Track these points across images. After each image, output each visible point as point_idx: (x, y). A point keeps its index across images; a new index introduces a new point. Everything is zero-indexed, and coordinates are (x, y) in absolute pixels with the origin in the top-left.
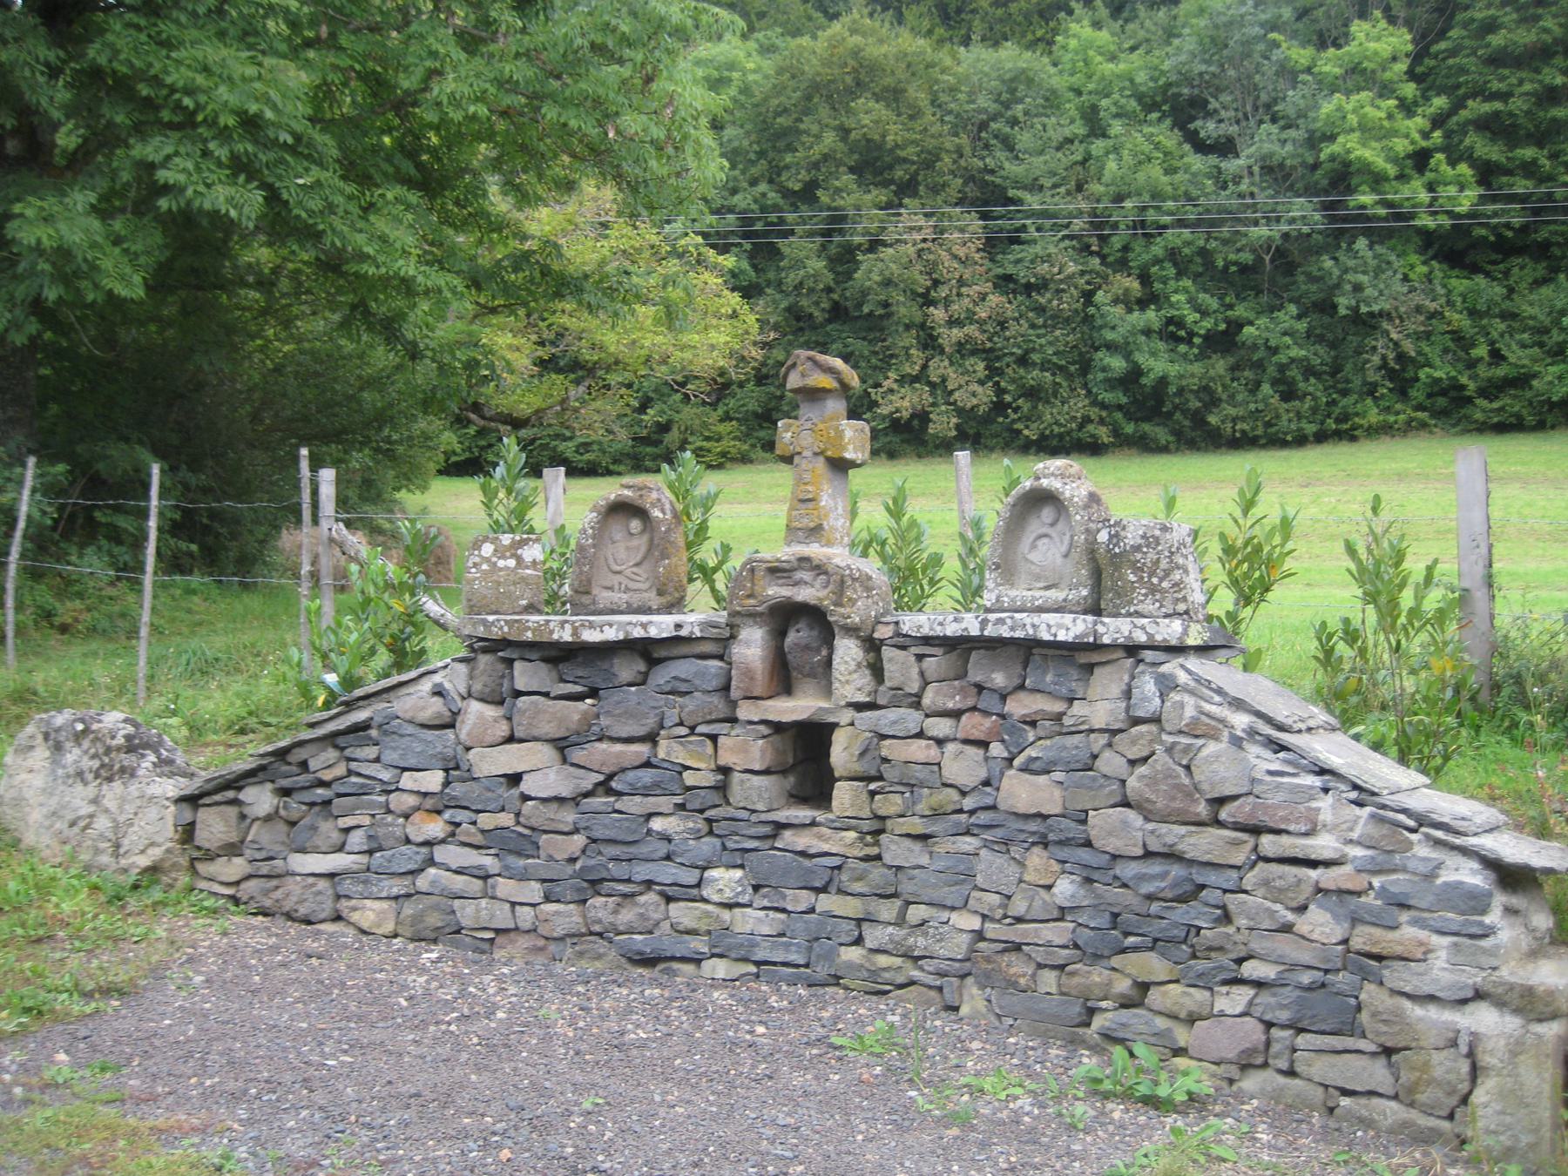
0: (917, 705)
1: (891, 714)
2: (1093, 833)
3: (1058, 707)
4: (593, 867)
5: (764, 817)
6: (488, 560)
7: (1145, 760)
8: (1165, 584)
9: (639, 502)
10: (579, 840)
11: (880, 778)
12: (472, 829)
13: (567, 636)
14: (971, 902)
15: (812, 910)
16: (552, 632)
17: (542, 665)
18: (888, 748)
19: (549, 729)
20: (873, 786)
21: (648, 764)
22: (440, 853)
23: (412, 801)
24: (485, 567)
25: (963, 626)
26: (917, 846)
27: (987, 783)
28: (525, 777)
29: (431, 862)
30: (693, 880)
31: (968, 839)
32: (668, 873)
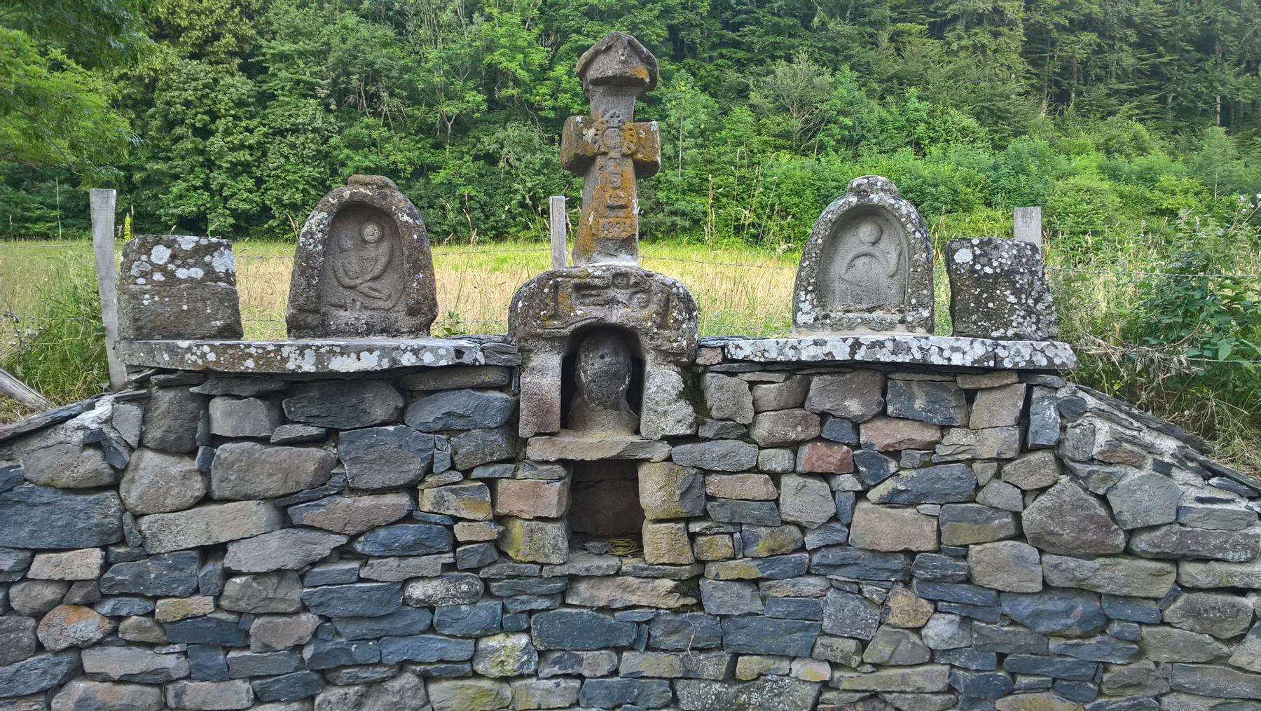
0: (746, 437)
1: (719, 448)
2: (977, 569)
3: (930, 435)
4: (329, 653)
5: (558, 571)
6: (162, 269)
7: (1043, 490)
8: (1040, 306)
9: (378, 203)
10: (309, 621)
11: (705, 516)
12: (148, 622)
13: (308, 366)
14: (817, 651)
15: (615, 673)
16: (287, 360)
17: (259, 402)
18: (715, 485)
19: (273, 485)
20: (695, 527)
21: (409, 518)
22: (91, 661)
23: (49, 593)
24: (158, 277)
25: (826, 349)
26: (747, 592)
27: (835, 518)
28: (231, 548)
29: (78, 672)
30: (465, 655)
31: (812, 580)
32: (434, 648)
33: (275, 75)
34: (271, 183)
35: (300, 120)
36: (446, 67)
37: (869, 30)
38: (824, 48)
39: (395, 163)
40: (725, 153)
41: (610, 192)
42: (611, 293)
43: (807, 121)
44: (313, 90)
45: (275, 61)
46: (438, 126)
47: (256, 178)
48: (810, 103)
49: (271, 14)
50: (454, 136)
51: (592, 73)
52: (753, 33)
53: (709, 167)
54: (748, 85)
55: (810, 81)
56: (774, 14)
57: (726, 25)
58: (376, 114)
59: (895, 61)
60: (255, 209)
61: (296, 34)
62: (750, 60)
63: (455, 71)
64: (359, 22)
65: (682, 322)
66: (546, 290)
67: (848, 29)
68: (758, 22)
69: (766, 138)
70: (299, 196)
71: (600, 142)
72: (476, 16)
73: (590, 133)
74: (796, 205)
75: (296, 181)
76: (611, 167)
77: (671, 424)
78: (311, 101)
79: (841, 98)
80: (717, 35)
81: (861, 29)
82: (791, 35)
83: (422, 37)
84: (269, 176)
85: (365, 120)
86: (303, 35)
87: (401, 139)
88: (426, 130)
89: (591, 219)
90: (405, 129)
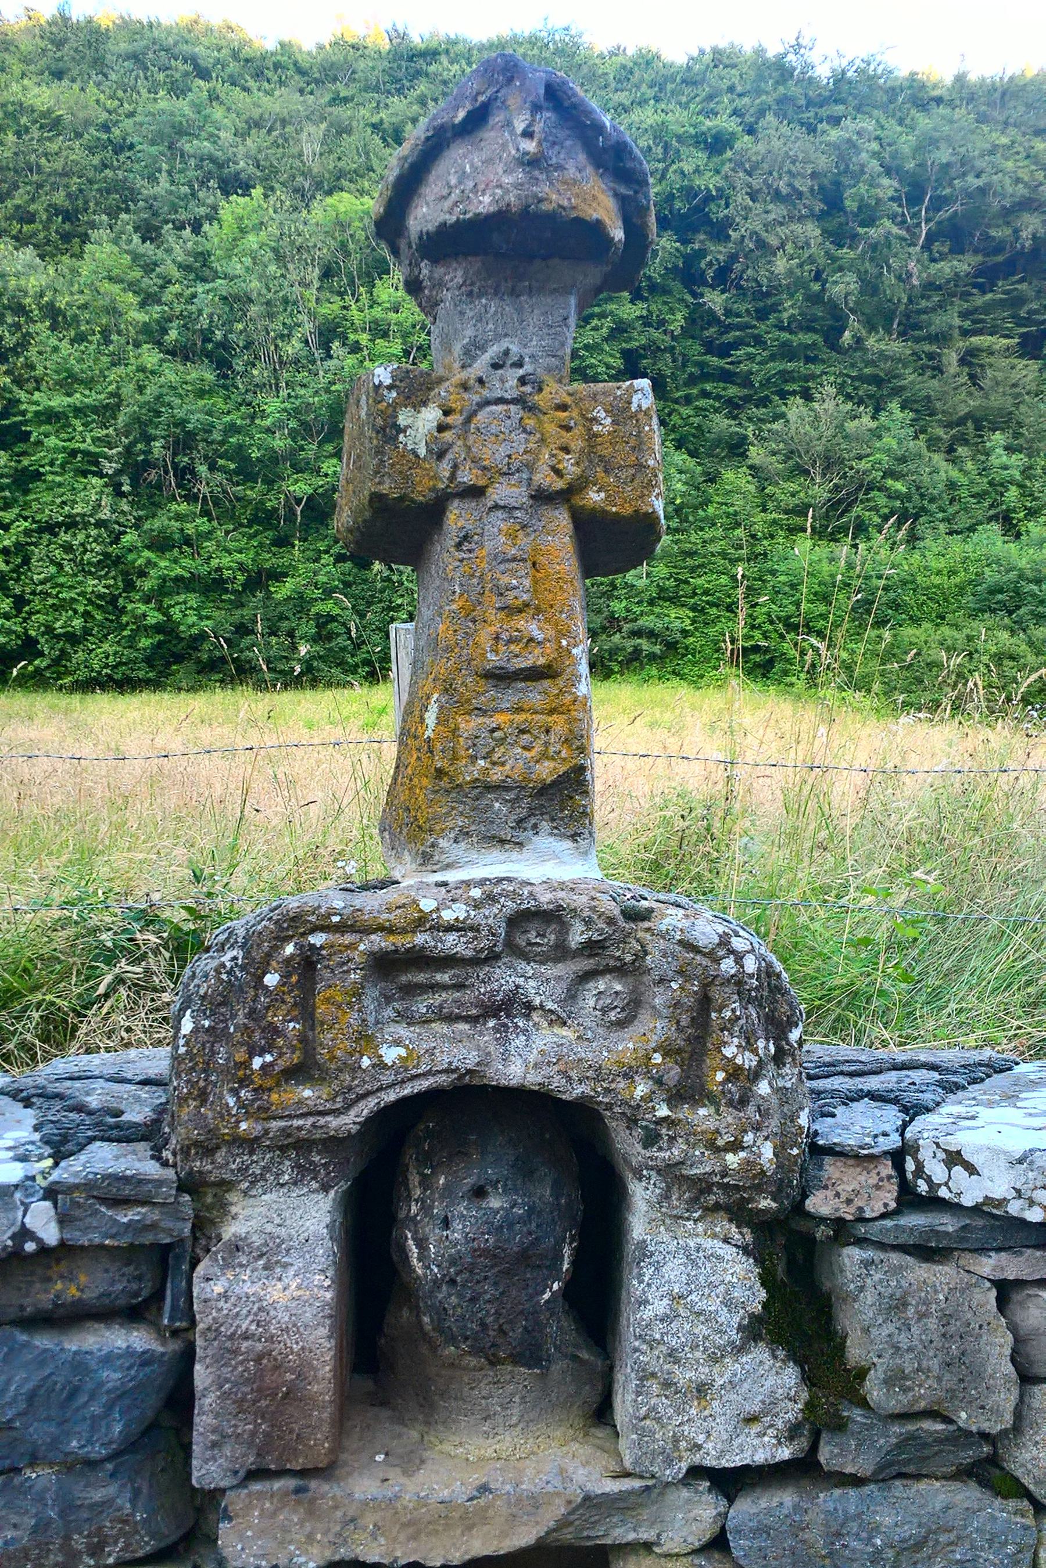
33: (39, 443)
34: (37, 604)
35: (78, 509)
36: (293, 424)
37: (927, 348)
38: (861, 378)
39: (219, 569)
40: (712, 540)
41: (495, 621)
42: (505, 977)
43: (837, 488)
44: (97, 463)
45: (41, 423)
46: (282, 512)
47: (15, 596)
48: (841, 461)
49: (32, 352)
50: (306, 528)
51: (426, 215)
52: (751, 357)
53: (690, 562)
54: (746, 437)
55: (841, 427)
56: (782, 329)
57: (710, 348)
58: (191, 498)
59: (970, 394)
60: (15, 643)
61: (69, 382)
62: (747, 399)
63: (306, 430)
64: (162, 361)
65: (755, 1075)
66: (271, 980)
67: (896, 347)
68: (758, 341)
69: (774, 515)
70: (78, 623)
71: (457, 450)
72: (335, 345)
73: (421, 423)
74: (824, 617)
75: (73, 600)
76: (496, 534)
77: (721, 1427)
78: (95, 480)
79: (888, 451)
80: (698, 364)
81: (917, 347)
82: (808, 360)
83: (257, 380)
84: (33, 593)
85: (174, 507)
86: (81, 382)
87: (227, 533)
88: (264, 518)
89: (431, 718)
90: (232, 518)
